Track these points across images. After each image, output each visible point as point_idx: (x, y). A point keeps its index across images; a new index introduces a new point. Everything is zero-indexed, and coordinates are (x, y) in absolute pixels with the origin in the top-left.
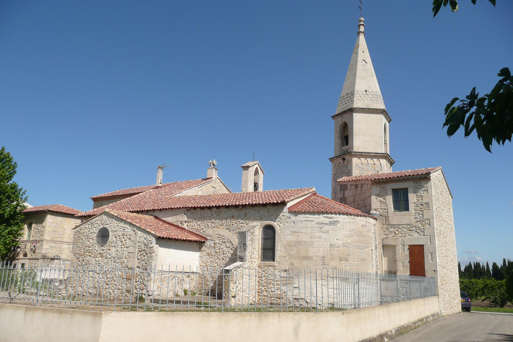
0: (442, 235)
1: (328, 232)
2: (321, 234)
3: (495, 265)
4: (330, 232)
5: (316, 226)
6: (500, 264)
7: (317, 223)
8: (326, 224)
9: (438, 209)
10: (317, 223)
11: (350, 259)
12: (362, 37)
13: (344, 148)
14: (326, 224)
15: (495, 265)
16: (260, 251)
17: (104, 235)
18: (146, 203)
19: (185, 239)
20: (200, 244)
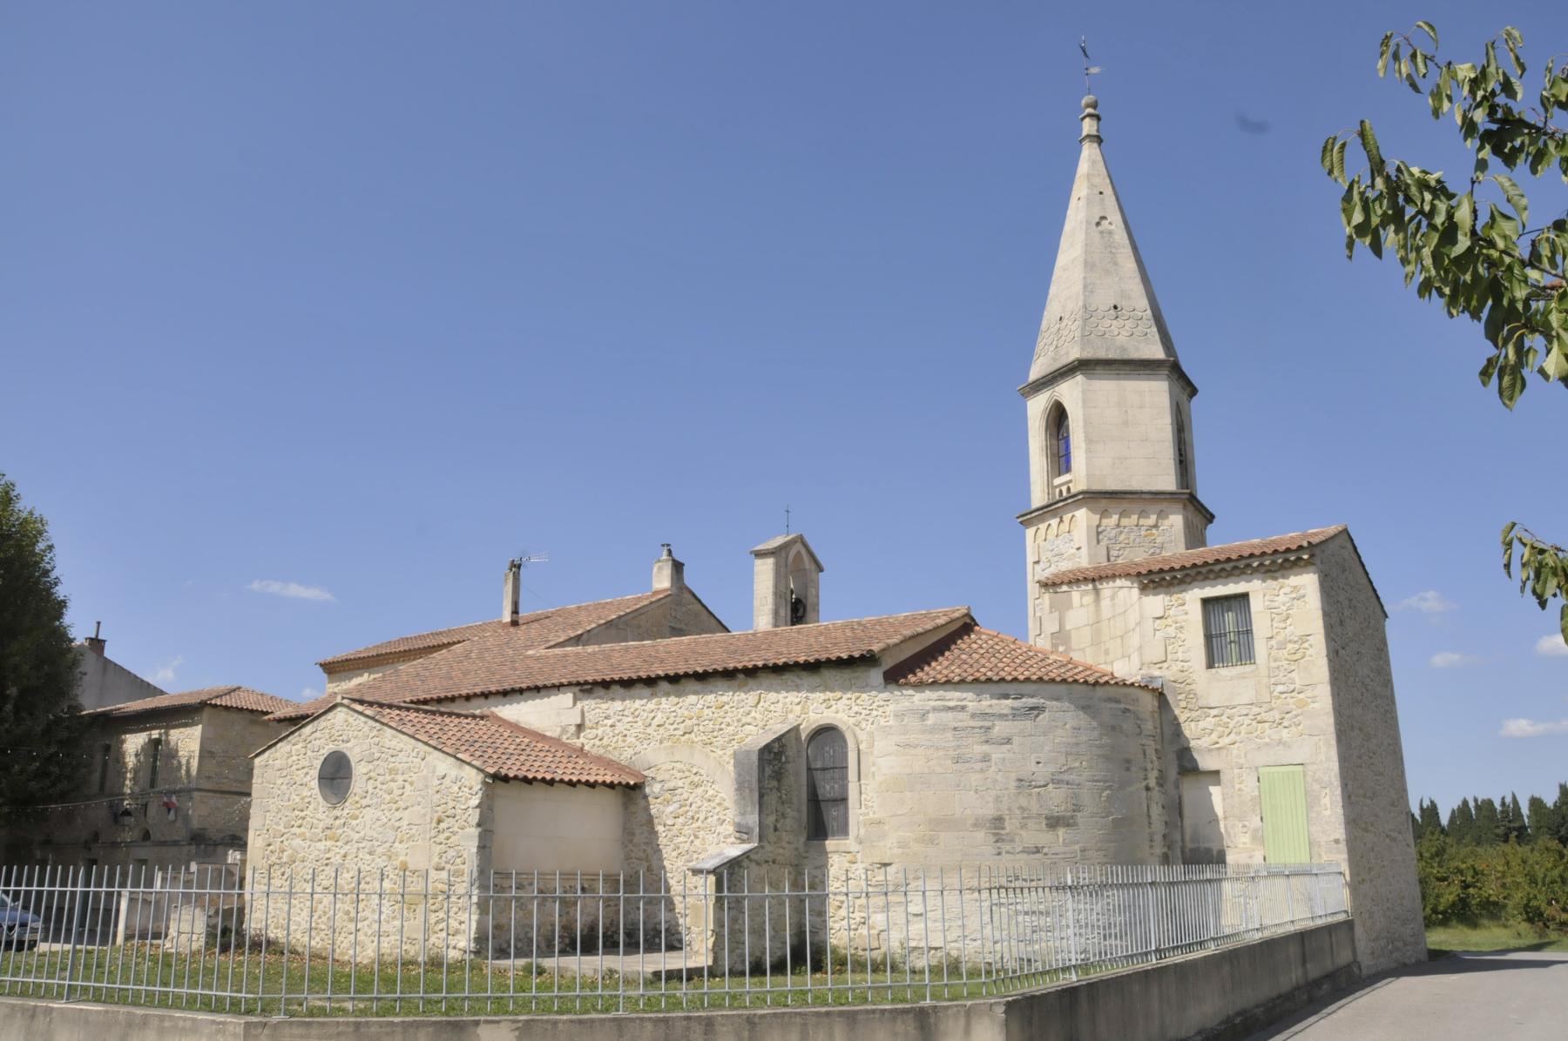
0: (1357, 731)
1: (1008, 741)
2: (986, 748)
3: (1536, 803)
4: (1016, 740)
5: (972, 723)
6: (1551, 798)
7: (973, 716)
8: (1003, 717)
9: (1342, 652)
10: (973, 716)
11: (1079, 820)
12: (130, 765)
13: (1057, 481)
14: (1003, 717)
15: (1536, 803)
16: (804, 808)
17: (335, 774)
18: (465, 674)
19: (575, 779)
20: (624, 794)
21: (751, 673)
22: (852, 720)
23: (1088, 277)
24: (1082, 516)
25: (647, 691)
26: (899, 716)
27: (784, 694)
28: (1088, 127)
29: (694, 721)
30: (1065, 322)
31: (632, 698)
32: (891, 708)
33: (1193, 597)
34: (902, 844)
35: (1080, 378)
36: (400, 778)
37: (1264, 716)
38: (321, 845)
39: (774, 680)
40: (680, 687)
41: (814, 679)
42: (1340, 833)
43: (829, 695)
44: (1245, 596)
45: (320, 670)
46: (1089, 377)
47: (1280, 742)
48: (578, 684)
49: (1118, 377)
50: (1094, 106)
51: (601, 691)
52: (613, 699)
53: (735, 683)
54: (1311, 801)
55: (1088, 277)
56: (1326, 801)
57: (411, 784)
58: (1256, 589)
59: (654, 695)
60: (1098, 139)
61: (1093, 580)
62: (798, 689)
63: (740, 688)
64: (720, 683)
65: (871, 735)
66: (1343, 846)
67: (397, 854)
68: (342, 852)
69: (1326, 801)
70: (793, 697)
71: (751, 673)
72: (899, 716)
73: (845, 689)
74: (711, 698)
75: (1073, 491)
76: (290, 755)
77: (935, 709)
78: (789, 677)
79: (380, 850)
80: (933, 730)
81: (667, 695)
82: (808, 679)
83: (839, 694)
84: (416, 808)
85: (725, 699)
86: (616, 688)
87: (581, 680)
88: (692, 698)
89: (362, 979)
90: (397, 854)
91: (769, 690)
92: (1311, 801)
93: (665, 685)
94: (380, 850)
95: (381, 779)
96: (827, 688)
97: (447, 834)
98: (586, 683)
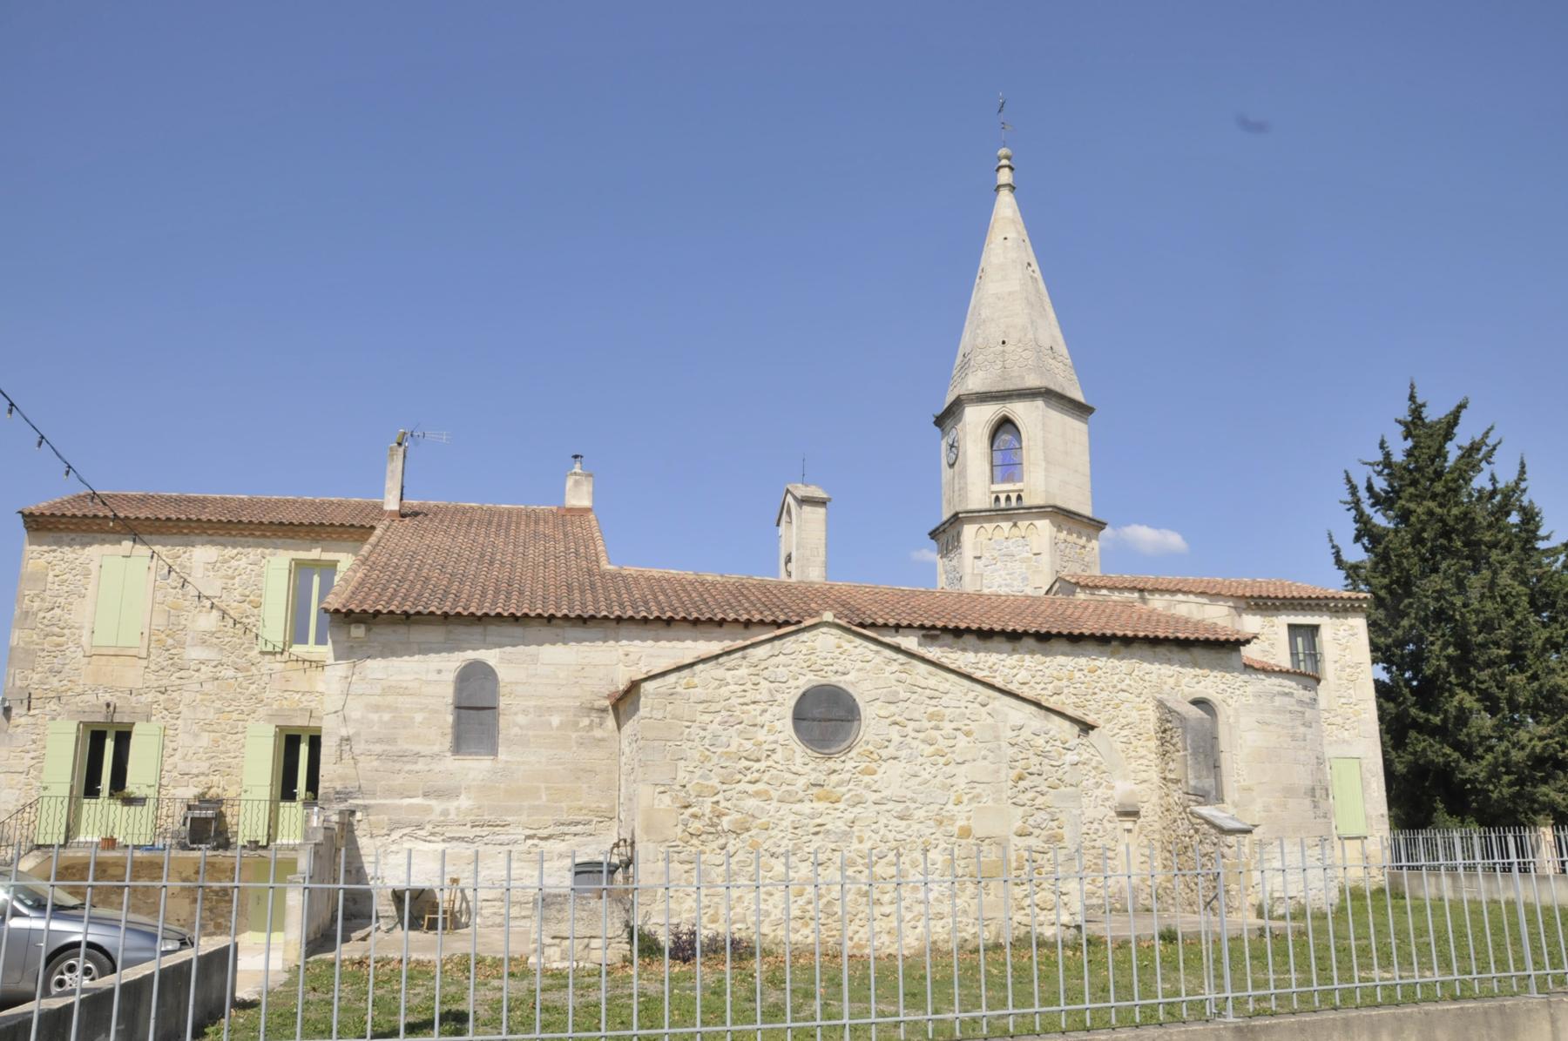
17: (825, 716)
21: (1127, 641)
22: (1220, 697)
23: (1009, 305)
24: (1044, 525)
25: (1008, 646)
26: (1258, 696)
27: (1157, 665)
28: (1005, 176)
29: (1065, 682)
30: (1008, 347)
31: (988, 651)
32: (1249, 689)
33: (1283, 620)
34: (1267, 809)
35: (1040, 403)
36: (948, 727)
37: (1332, 720)
38: (806, 808)
39: (1147, 651)
40: (1046, 646)
41: (1185, 656)
42: (1384, 809)
43: (1198, 671)
44: (1314, 629)
45: (20, 519)
46: (1048, 404)
47: (1344, 741)
48: (922, 627)
49: (1062, 411)
50: (1008, 158)
51: (949, 639)
52: (964, 650)
53: (1109, 649)
54: (1365, 787)
55: (1009, 305)
56: (1374, 786)
57: (967, 734)
58: (1323, 620)
59: (1014, 651)
60: (1012, 188)
61: (1141, 591)
62: (1169, 662)
63: (1112, 655)
64: (1090, 647)
65: (1236, 710)
66: (1386, 819)
67: (952, 818)
68: (849, 816)
69: (1374, 786)
70: (1166, 670)
71: (1127, 641)
72: (1258, 696)
73: (1212, 668)
74: (1083, 661)
75: (1026, 502)
76: (723, 683)
77: (1279, 694)
78: (1161, 650)
79: (921, 814)
80: (1278, 711)
81: (1032, 652)
82: (1177, 654)
83: (1206, 672)
84: (981, 763)
85: (1098, 663)
86: (970, 640)
87: (928, 623)
88: (1061, 659)
89: (914, 979)
90: (952, 818)
91: (1143, 659)
92: (1365, 787)
93: (1031, 642)
94: (921, 814)
95: (911, 725)
96: (1195, 665)
97: (1030, 794)
98: (934, 627)
